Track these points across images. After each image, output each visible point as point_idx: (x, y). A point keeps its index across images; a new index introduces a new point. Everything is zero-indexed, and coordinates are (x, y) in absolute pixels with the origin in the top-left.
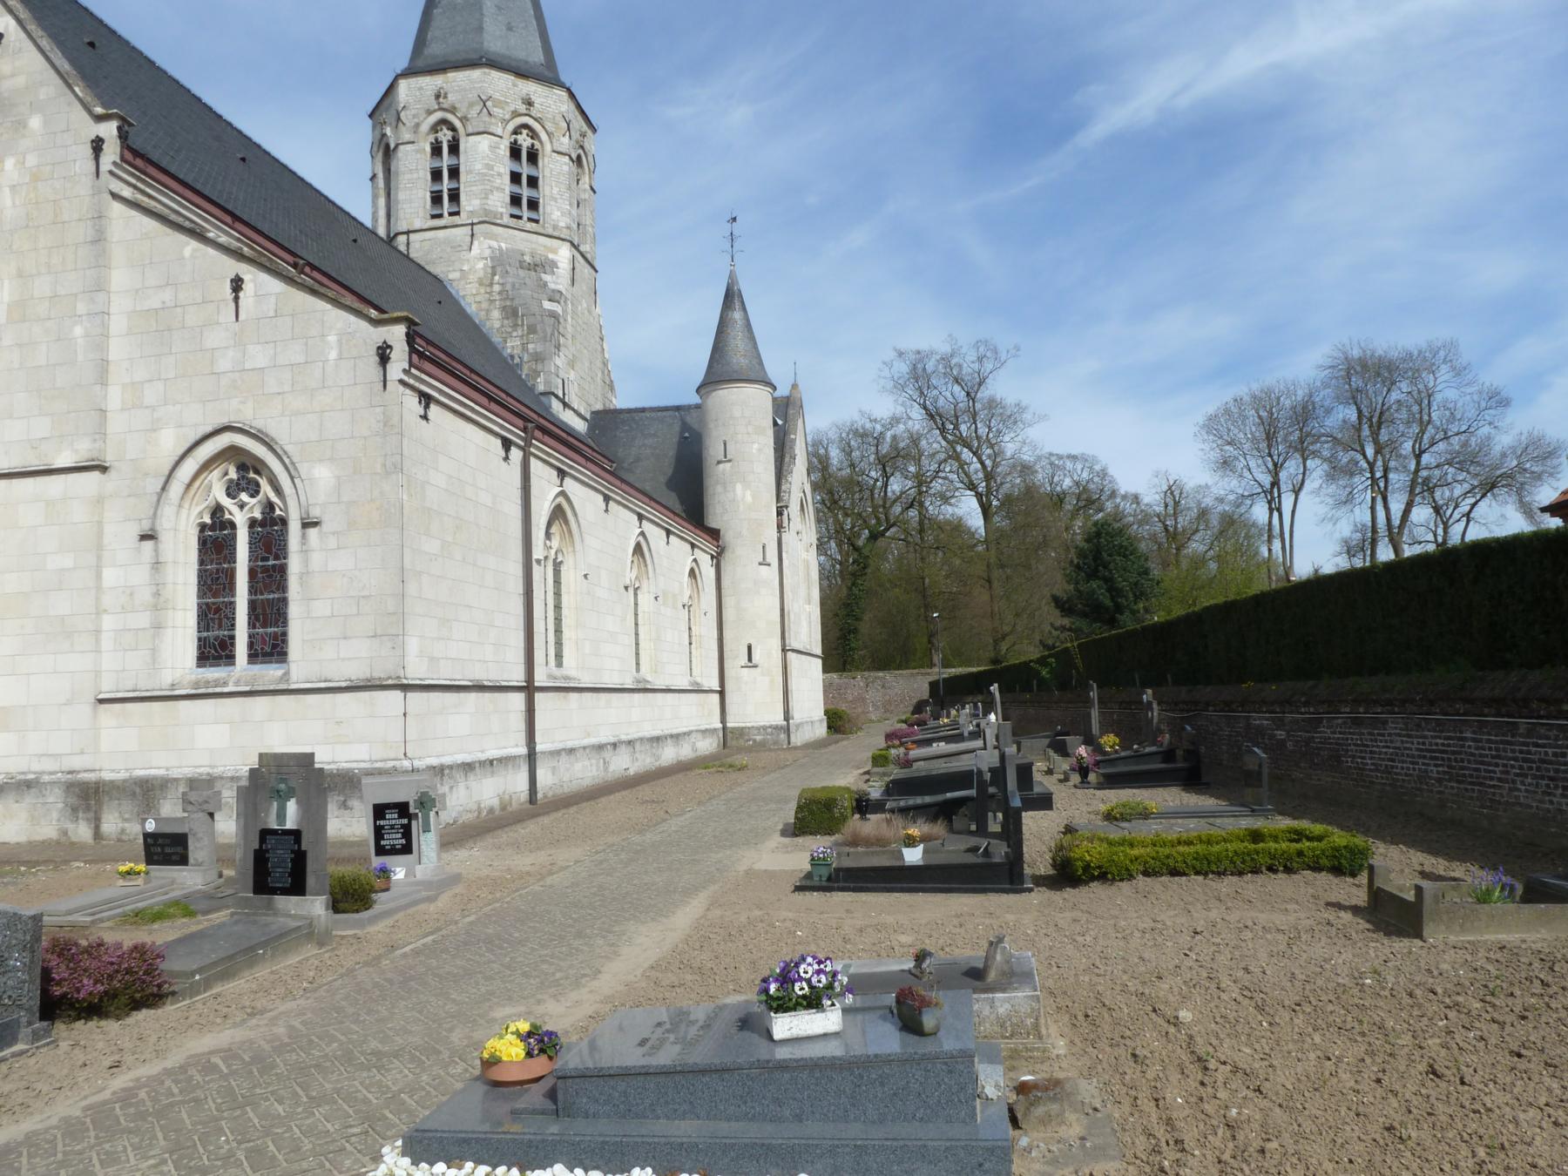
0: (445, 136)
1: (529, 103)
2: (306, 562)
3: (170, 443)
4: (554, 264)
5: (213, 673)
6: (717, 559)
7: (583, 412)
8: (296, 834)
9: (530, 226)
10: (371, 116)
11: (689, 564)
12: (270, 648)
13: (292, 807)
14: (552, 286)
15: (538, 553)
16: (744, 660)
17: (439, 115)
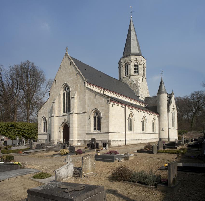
0: (126, 65)
2: (102, 121)
3: (91, 110)
4: (140, 80)
6: (159, 117)
7: (144, 98)
8: (94, 144)
10: (118, 63)
11: (153, 117)
13: (94, 142)
14: (139, 82)
17: (126, 63)
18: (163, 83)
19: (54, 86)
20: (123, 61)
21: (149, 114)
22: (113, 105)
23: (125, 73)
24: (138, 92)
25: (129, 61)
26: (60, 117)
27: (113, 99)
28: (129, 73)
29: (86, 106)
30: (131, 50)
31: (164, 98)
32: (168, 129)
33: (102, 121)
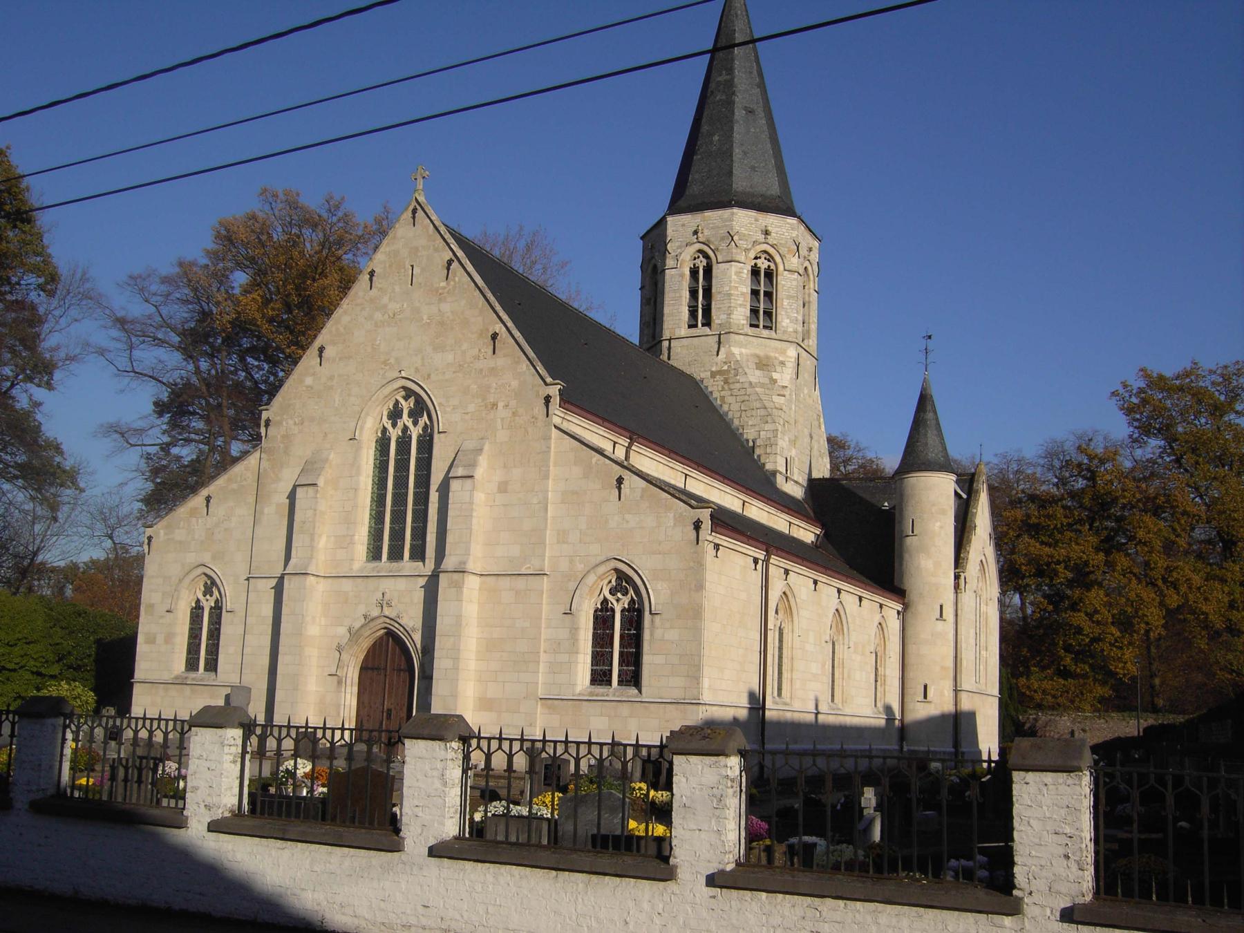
1: (767, 233)
5: (601, 690)
9: (766, 333)
10: (642, 238)
11: (877, 618)
12: (633, 678)
14: (780, 383)
15: (770, 626)
16: (921, 698)
18: (935, 412)
19: (309, 381)
20: (679, 227)
21: (860, 599)
22: (717, 547)
23: (693, 313)
24: (771, 443)
25: (722, 239)
26: (347, 585)
27: (726, 522)
28: (717, 317)
29: (550, 536)
30: (730, 173)
31: (934, 494)
32: (956, 691)
33: (652, 635)
